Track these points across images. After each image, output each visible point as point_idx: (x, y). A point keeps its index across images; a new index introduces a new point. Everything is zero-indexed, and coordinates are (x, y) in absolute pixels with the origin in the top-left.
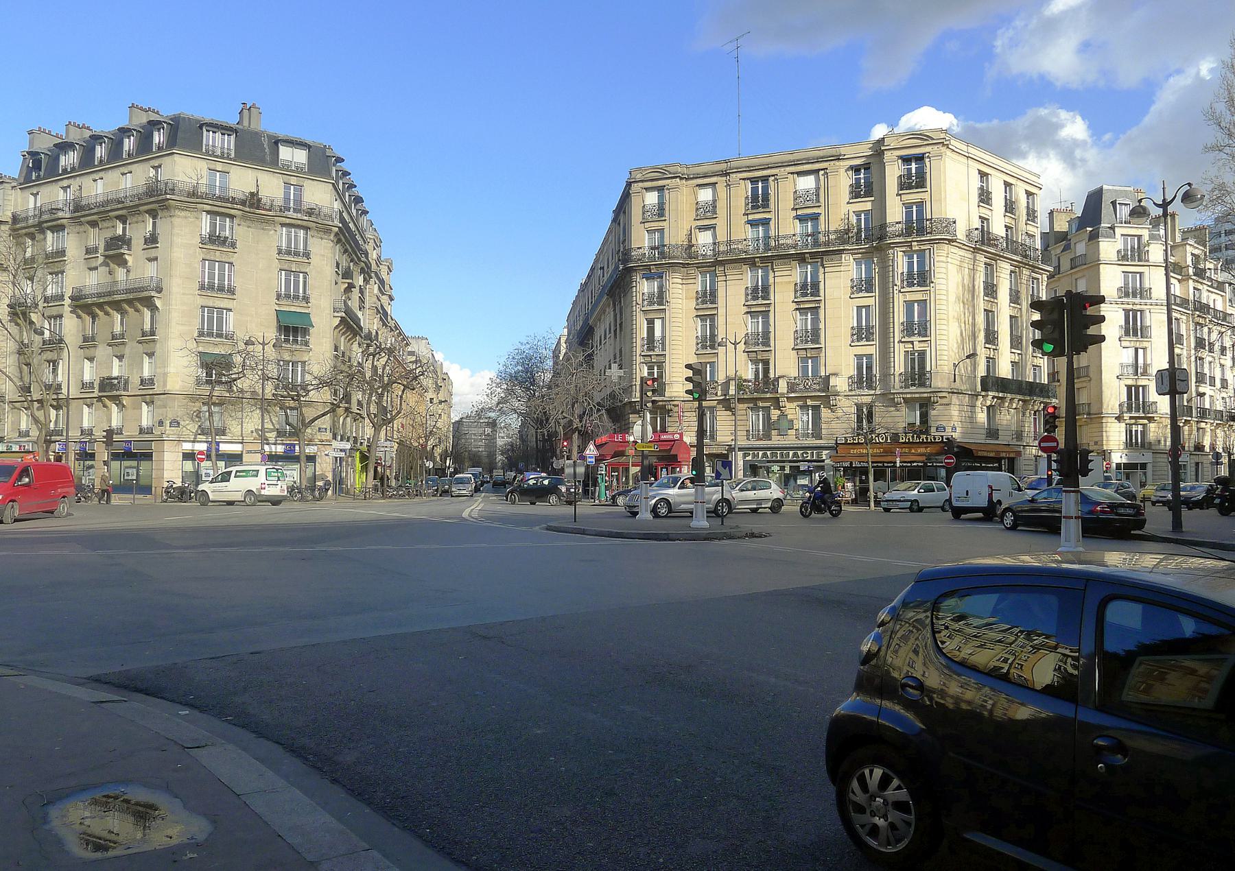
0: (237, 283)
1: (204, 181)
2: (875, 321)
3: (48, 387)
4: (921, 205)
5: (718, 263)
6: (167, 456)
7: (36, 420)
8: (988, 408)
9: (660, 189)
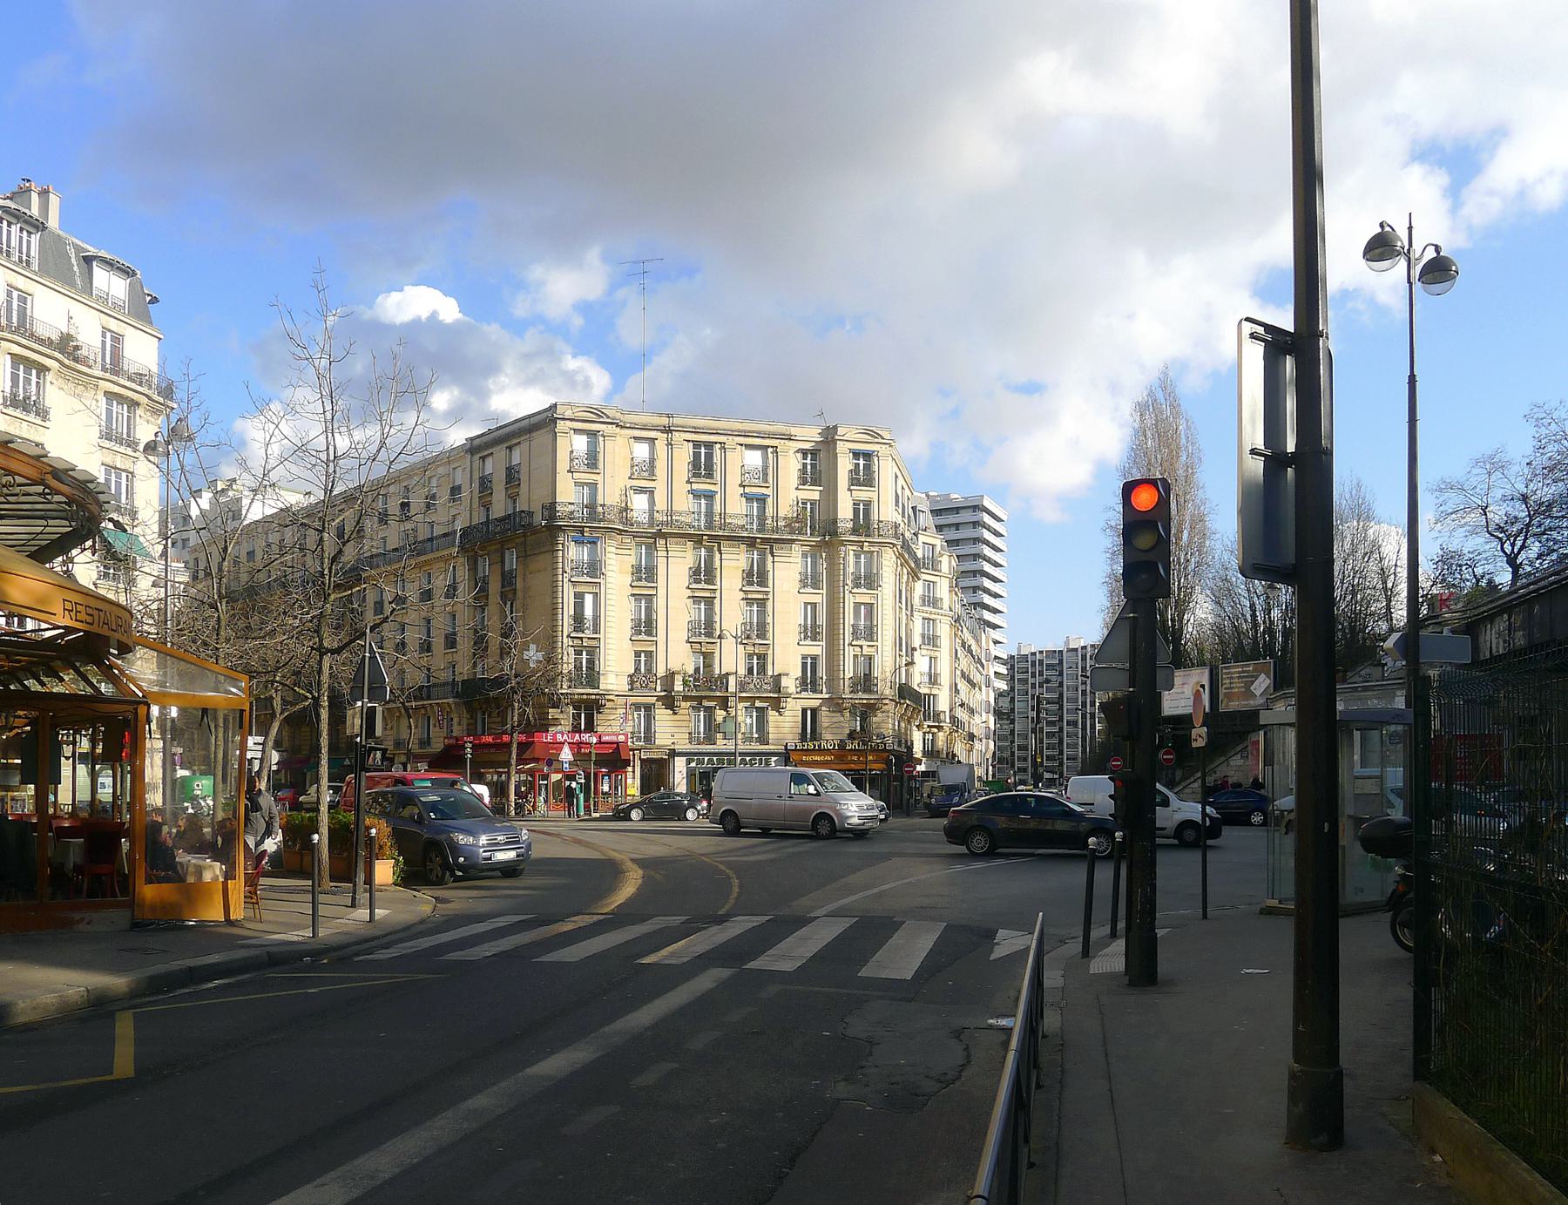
2: (822, 620)
4: (868, 504)
9: (592, 434)
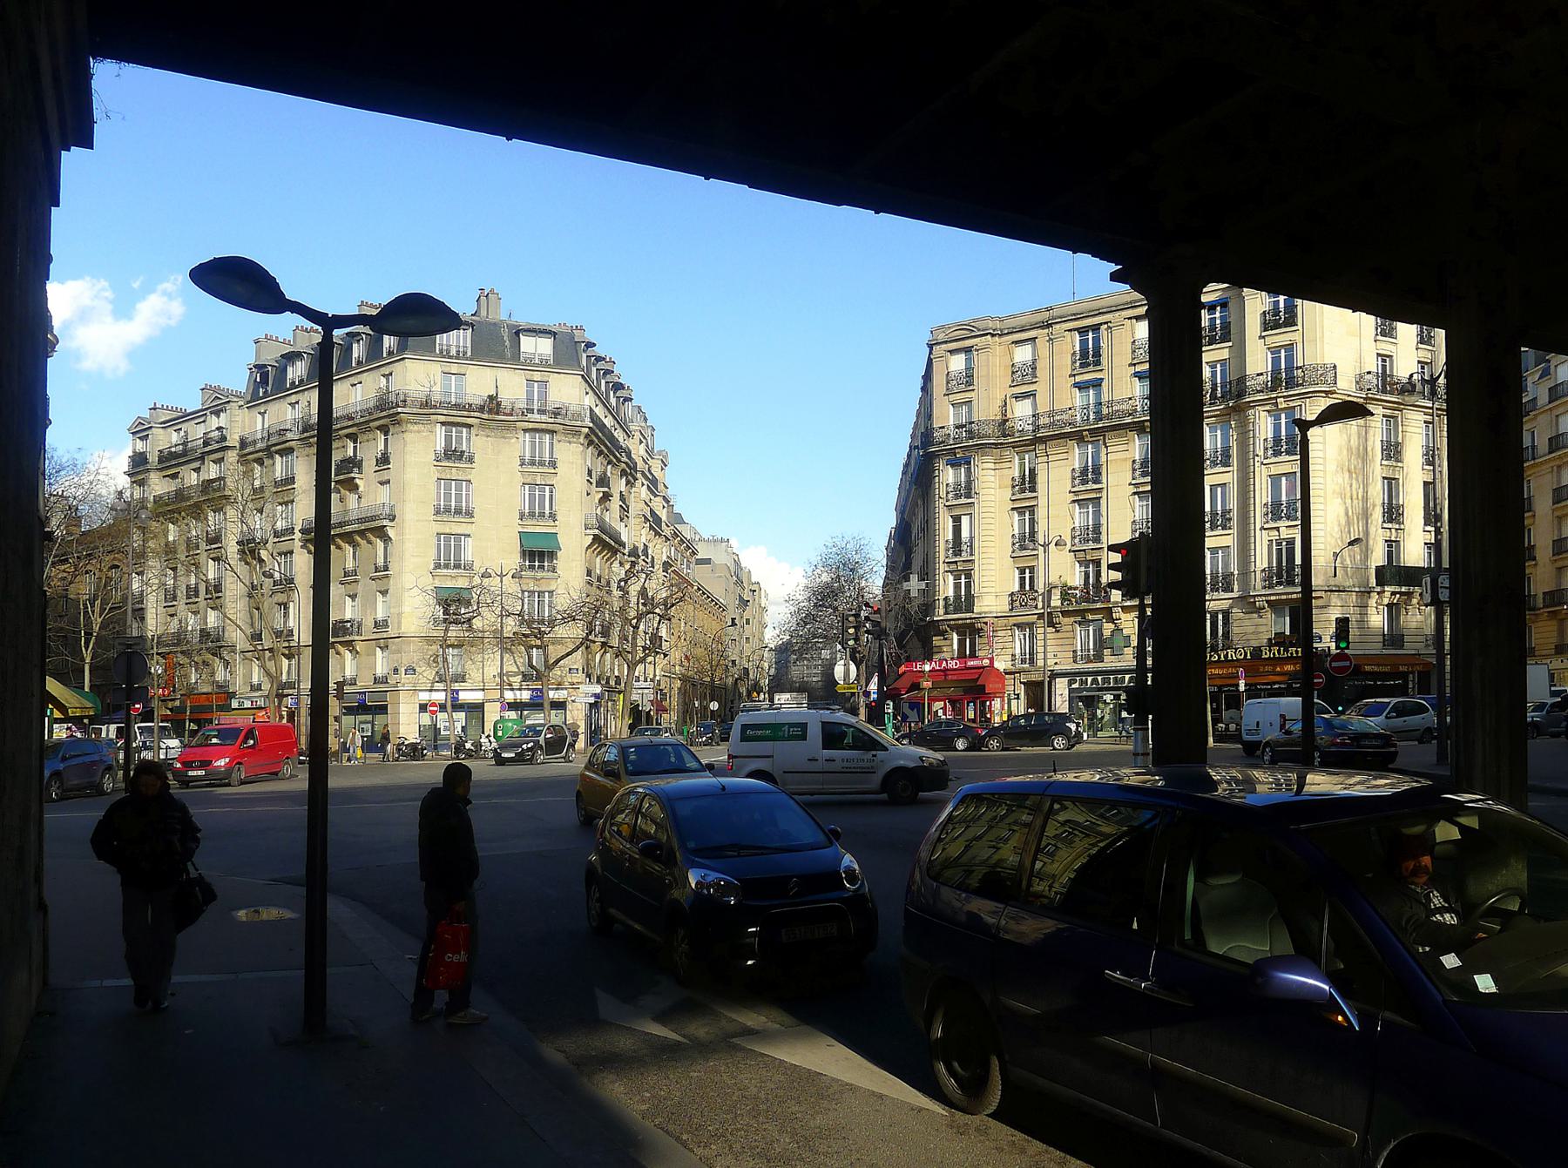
0: (477, 503)
1: (437, 388)
3: (278, 634)
4: (1290, 348)
5: (1039, 440)
6: (402, 708)
7: (268, 674)
8: (1390, 606)
9: (968, 350)
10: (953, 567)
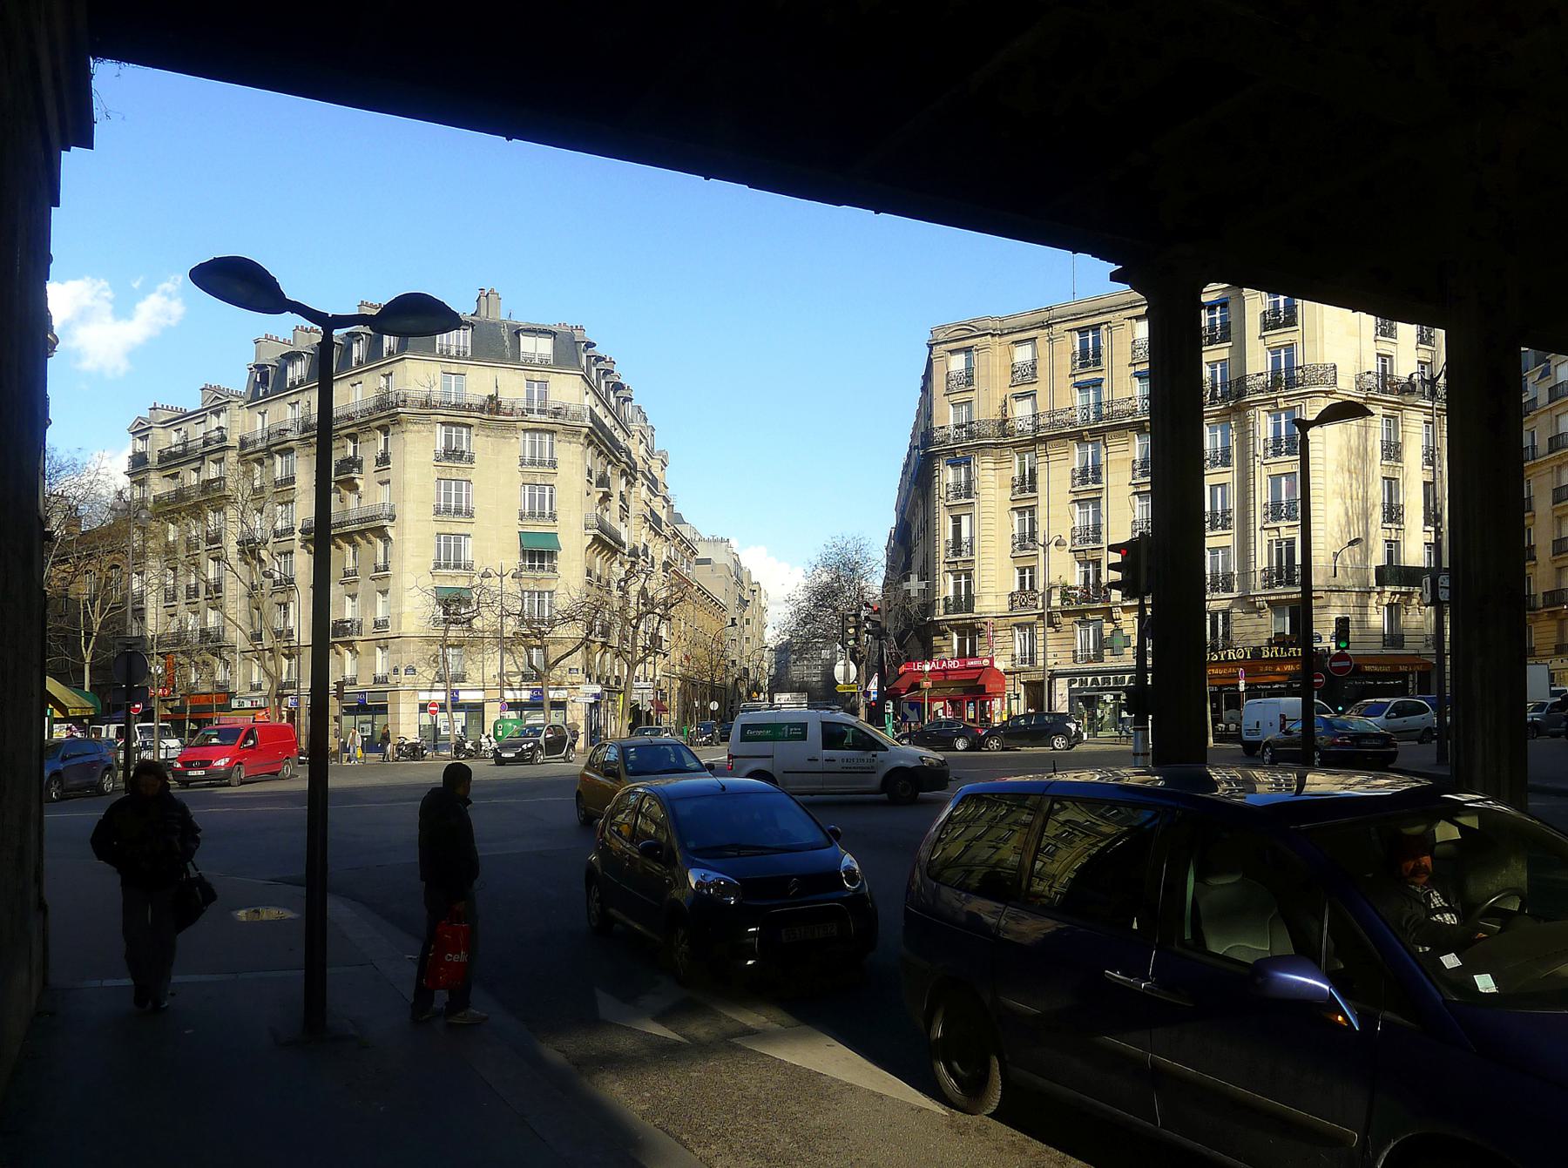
0: (477, 503)
1: (437, 388)
3: (278, 634)
4: (1290, 348)
5: (1039, 440)
6: (402, 708)
7: (268, 674)
8: (1390, 606)
9: (968, 350)
10: (953, 567)
